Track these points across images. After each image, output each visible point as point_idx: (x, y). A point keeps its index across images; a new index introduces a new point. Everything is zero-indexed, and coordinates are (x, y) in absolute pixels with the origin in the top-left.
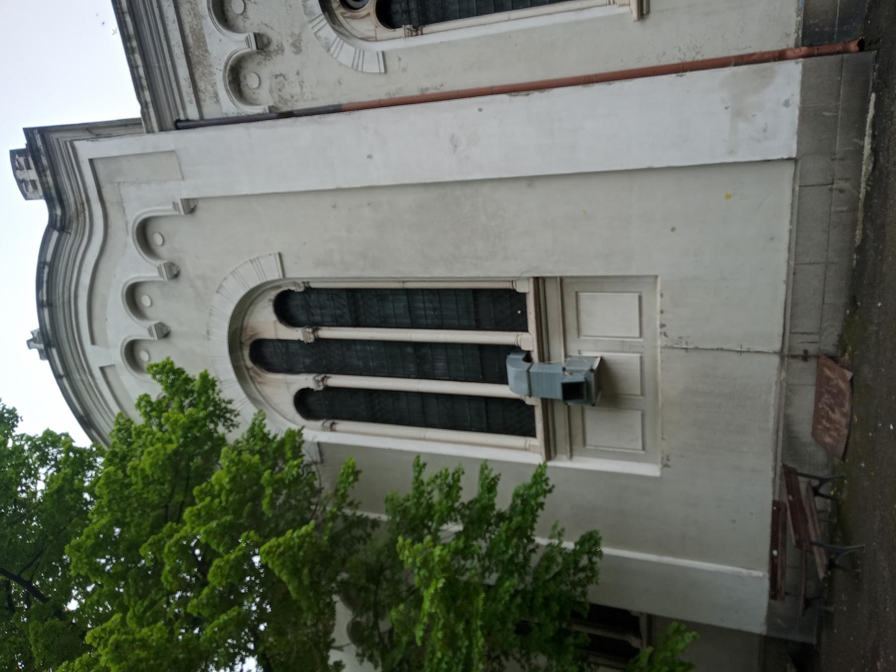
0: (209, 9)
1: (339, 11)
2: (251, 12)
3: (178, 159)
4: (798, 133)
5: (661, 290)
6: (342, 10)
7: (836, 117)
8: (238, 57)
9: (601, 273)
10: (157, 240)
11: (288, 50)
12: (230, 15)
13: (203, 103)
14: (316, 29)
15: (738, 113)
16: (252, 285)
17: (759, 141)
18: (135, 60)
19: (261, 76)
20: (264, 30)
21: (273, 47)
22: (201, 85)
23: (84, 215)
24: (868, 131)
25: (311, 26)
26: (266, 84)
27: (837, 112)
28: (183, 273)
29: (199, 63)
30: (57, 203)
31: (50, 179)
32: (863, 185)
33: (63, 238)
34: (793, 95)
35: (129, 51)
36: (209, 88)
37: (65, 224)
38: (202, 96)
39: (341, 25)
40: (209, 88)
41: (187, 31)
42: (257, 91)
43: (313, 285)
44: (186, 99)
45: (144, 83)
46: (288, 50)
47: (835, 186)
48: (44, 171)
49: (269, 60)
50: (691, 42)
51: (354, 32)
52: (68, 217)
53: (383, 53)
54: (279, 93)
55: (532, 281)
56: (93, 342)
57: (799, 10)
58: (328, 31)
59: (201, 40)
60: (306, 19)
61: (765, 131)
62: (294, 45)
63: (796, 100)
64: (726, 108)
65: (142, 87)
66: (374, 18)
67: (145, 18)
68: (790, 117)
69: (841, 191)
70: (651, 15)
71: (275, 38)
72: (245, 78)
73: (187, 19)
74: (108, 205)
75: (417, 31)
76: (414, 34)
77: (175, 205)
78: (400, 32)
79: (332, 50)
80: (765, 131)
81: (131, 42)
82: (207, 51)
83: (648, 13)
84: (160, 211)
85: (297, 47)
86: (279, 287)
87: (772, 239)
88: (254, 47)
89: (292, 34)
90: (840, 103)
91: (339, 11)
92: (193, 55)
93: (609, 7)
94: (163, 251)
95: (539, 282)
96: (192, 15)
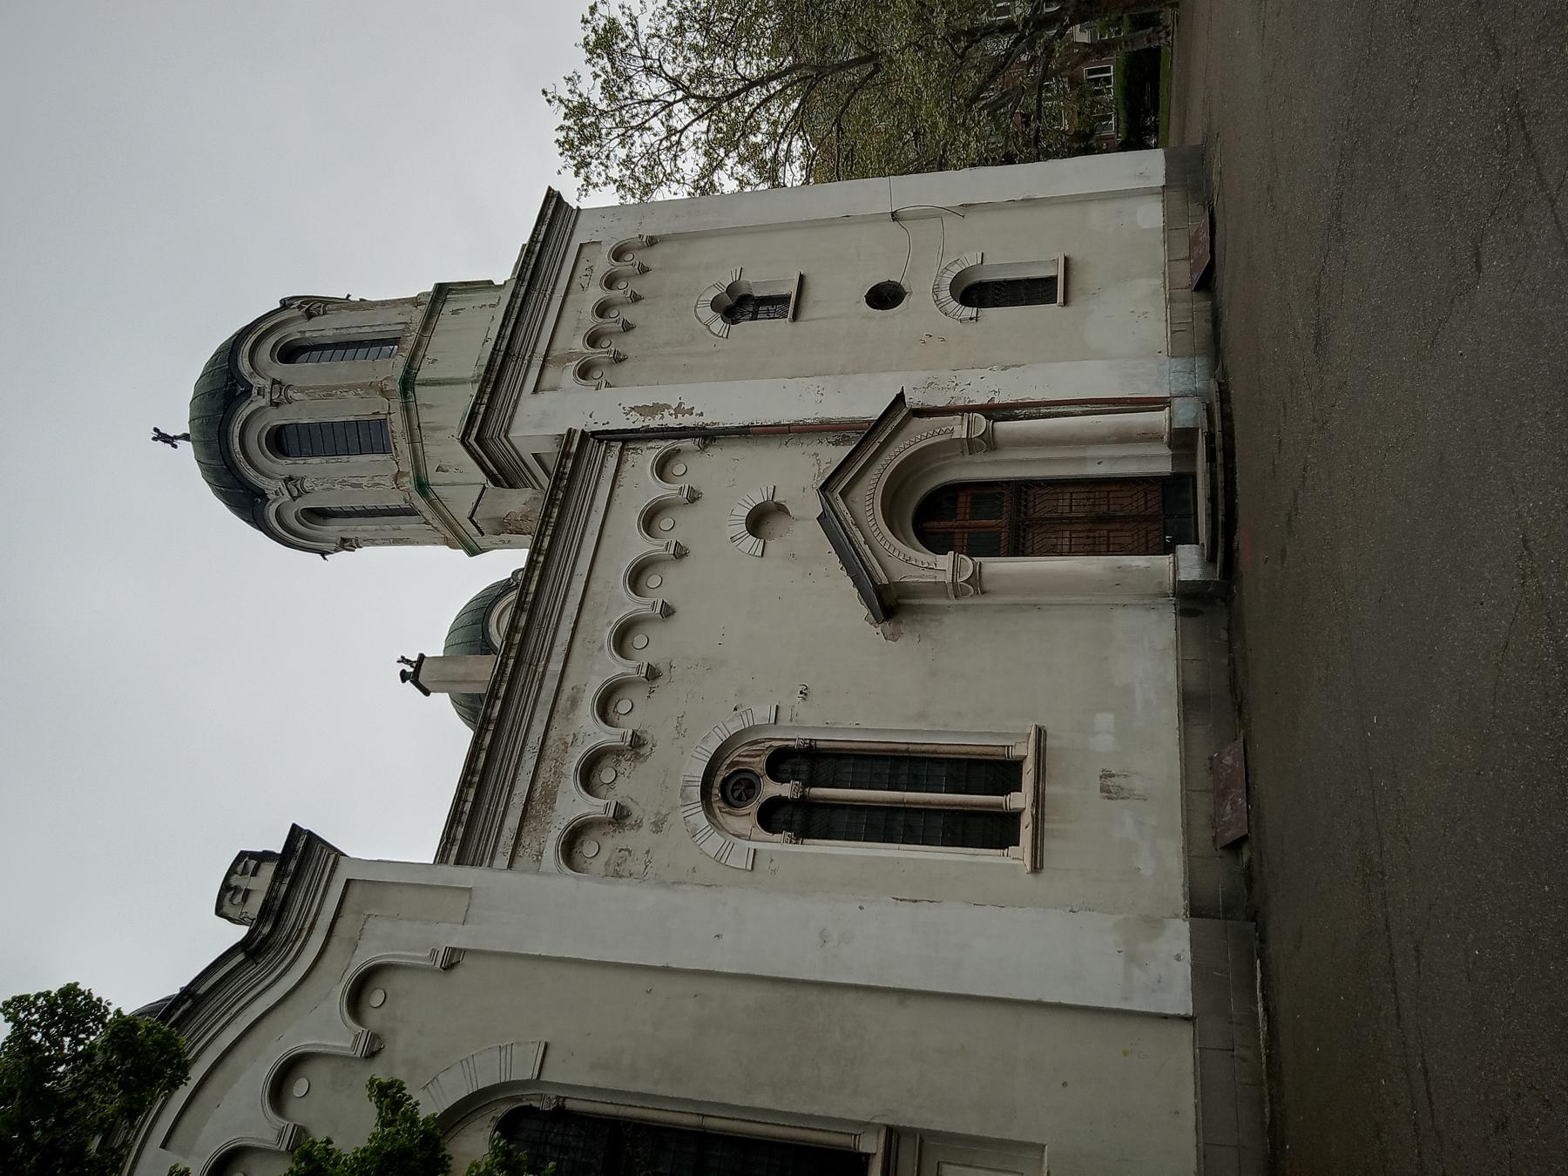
0: (576, 770)
1: (717, 805)
2: (618, 785)
3: (470, 898)
4: (1192, 989)
5: (1048, 1167)
6: (721, 805)
7: (1228, 978)
8: (369, 968)
9: (974, 1131)
10: (377, 998)
11: (647, 827)
12: (595, 781)
13: (517, 859)
14: (687, 814)
15: (1131, 959)
16: (483, 1083)
17: (1154, 991)
18: (467, 793)
19: (601, 847)
20: (627, 802)
21: (631, 821)
22: (526, 840)
23: (293, 946)
24: (1259, 994)
25: (683, 810)
26: (604, 856)
27: (1228, 974)
28: (385, 1054)
29: (535, 817)
30: (272, 918)
31: (284, 888)
32: (1263, 1051)
33: (248, 964)
34: (1183, 951)
35: (464, 783)
36: (535, 845)
37: (261, 949)
38: (521, 851)
39: (715, 816)
40: (535, 845)
41: (539, 784)
42: (589, 861)
43: (570, 1105)
44: (500, 849)
45: (464, 818)
46: (647, 827)
47: (1235, 1053)
48: (284, 876)
49: (620, 833)
50: (1083, 902)
51: (726, 827)
52: (272, 940)
53: (755, 850)
54: (617, 867)
55: (883, 1133)
56: (164, 1146)
57: (1185, 894)
58: (700, 818)
59: (550, 797)
60: (680, 802)
61: (1159, 981)
62: (655, 824)
63: (1187, 955)
64: (1119, 952)
65: (459, 821)
66: (754, 818)
67: (499, 761)
68: (1181, 975)
69: (1244, 1060)
70: (1044, 871)
71: (636, 812)
72: (582, 845)
73: (544, 774)
74: (334, 940)
75: (797, 839)
76: (794, 841)
77: (434, 952)
78: (777, 837)
79: (698, 837)
80: (1159, 981)
81: (473, 776)
82: (551, 808)
83: (1042, 868)
84: (408, 957)
85: (658, 827)
86: (518, 1099)
87: (1177, 1113)
88: (611, 815)
89: (658, 813)
90: (1229, 965)
91: (717, 805)
92: (532, 809)
93: (1002, 857)
94: (374, 1018)
95: (893, 1134)
96: (553, 772)
